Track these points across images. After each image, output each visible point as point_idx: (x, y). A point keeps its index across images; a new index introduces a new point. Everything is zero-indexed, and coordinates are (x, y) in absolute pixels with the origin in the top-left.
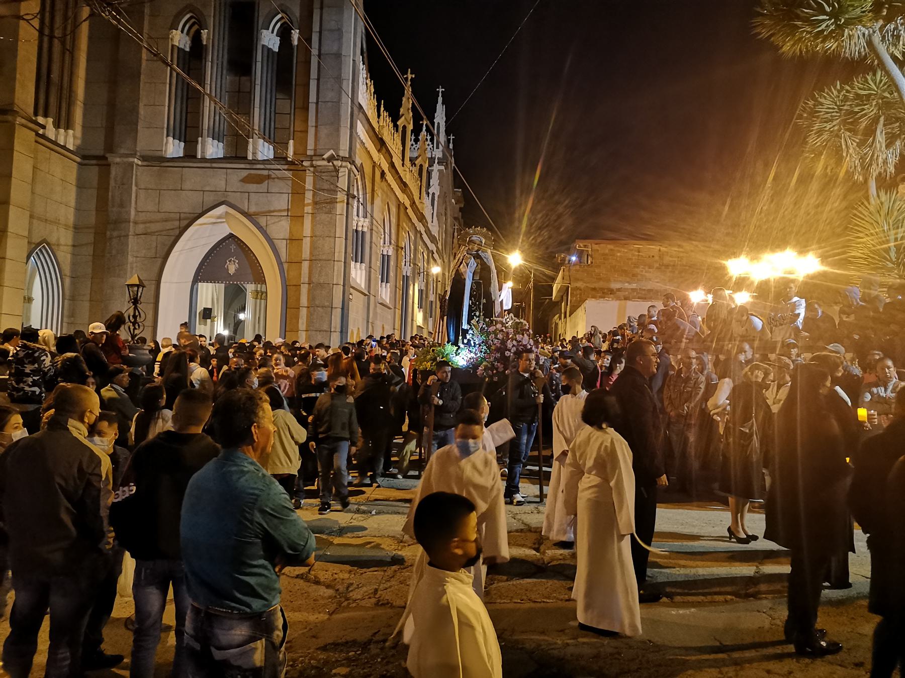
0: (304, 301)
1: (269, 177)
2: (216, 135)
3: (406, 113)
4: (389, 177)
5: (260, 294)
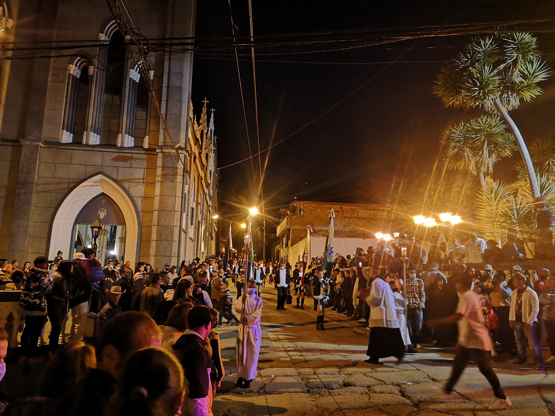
0: (154, 236)
1: (132, 158)
2: (96, 131)
3: (203, 123)
4: (197, 161)
5: (104, 231)
